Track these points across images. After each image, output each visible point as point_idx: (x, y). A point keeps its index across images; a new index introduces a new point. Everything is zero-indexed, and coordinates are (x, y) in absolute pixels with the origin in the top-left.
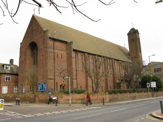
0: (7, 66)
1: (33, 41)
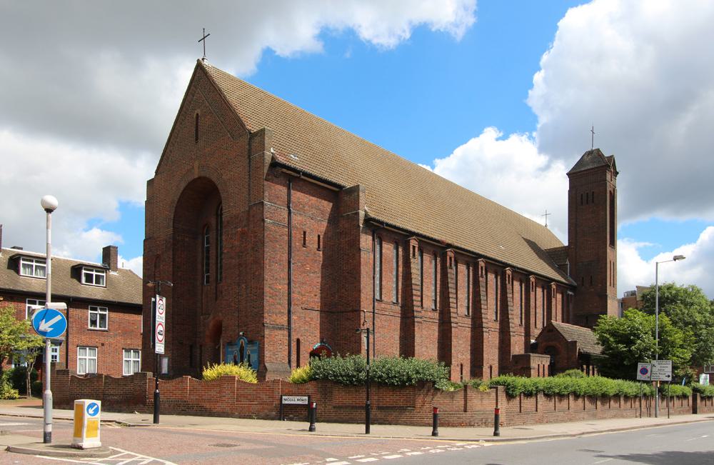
0: (94, 273)
1: (203, 174)
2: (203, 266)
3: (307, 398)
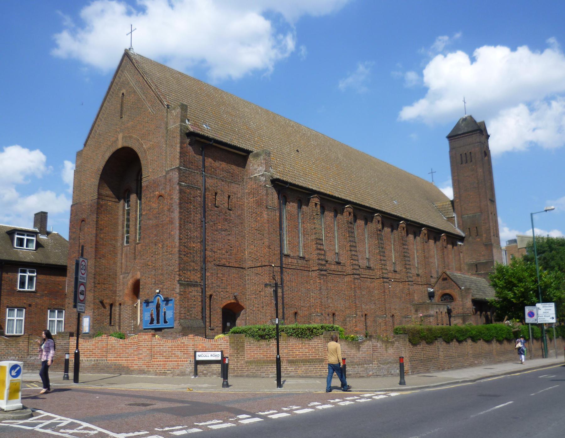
1: (126, 145)
2: (123, 228)
3: (220, 353)
